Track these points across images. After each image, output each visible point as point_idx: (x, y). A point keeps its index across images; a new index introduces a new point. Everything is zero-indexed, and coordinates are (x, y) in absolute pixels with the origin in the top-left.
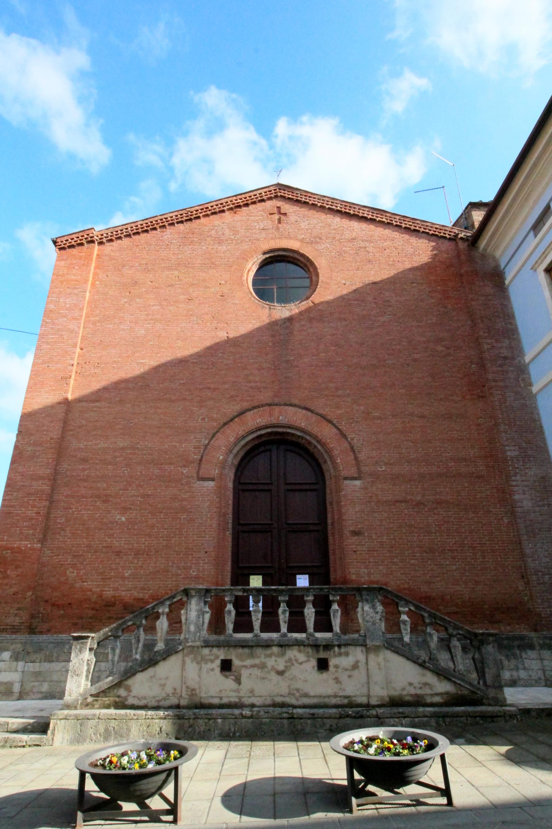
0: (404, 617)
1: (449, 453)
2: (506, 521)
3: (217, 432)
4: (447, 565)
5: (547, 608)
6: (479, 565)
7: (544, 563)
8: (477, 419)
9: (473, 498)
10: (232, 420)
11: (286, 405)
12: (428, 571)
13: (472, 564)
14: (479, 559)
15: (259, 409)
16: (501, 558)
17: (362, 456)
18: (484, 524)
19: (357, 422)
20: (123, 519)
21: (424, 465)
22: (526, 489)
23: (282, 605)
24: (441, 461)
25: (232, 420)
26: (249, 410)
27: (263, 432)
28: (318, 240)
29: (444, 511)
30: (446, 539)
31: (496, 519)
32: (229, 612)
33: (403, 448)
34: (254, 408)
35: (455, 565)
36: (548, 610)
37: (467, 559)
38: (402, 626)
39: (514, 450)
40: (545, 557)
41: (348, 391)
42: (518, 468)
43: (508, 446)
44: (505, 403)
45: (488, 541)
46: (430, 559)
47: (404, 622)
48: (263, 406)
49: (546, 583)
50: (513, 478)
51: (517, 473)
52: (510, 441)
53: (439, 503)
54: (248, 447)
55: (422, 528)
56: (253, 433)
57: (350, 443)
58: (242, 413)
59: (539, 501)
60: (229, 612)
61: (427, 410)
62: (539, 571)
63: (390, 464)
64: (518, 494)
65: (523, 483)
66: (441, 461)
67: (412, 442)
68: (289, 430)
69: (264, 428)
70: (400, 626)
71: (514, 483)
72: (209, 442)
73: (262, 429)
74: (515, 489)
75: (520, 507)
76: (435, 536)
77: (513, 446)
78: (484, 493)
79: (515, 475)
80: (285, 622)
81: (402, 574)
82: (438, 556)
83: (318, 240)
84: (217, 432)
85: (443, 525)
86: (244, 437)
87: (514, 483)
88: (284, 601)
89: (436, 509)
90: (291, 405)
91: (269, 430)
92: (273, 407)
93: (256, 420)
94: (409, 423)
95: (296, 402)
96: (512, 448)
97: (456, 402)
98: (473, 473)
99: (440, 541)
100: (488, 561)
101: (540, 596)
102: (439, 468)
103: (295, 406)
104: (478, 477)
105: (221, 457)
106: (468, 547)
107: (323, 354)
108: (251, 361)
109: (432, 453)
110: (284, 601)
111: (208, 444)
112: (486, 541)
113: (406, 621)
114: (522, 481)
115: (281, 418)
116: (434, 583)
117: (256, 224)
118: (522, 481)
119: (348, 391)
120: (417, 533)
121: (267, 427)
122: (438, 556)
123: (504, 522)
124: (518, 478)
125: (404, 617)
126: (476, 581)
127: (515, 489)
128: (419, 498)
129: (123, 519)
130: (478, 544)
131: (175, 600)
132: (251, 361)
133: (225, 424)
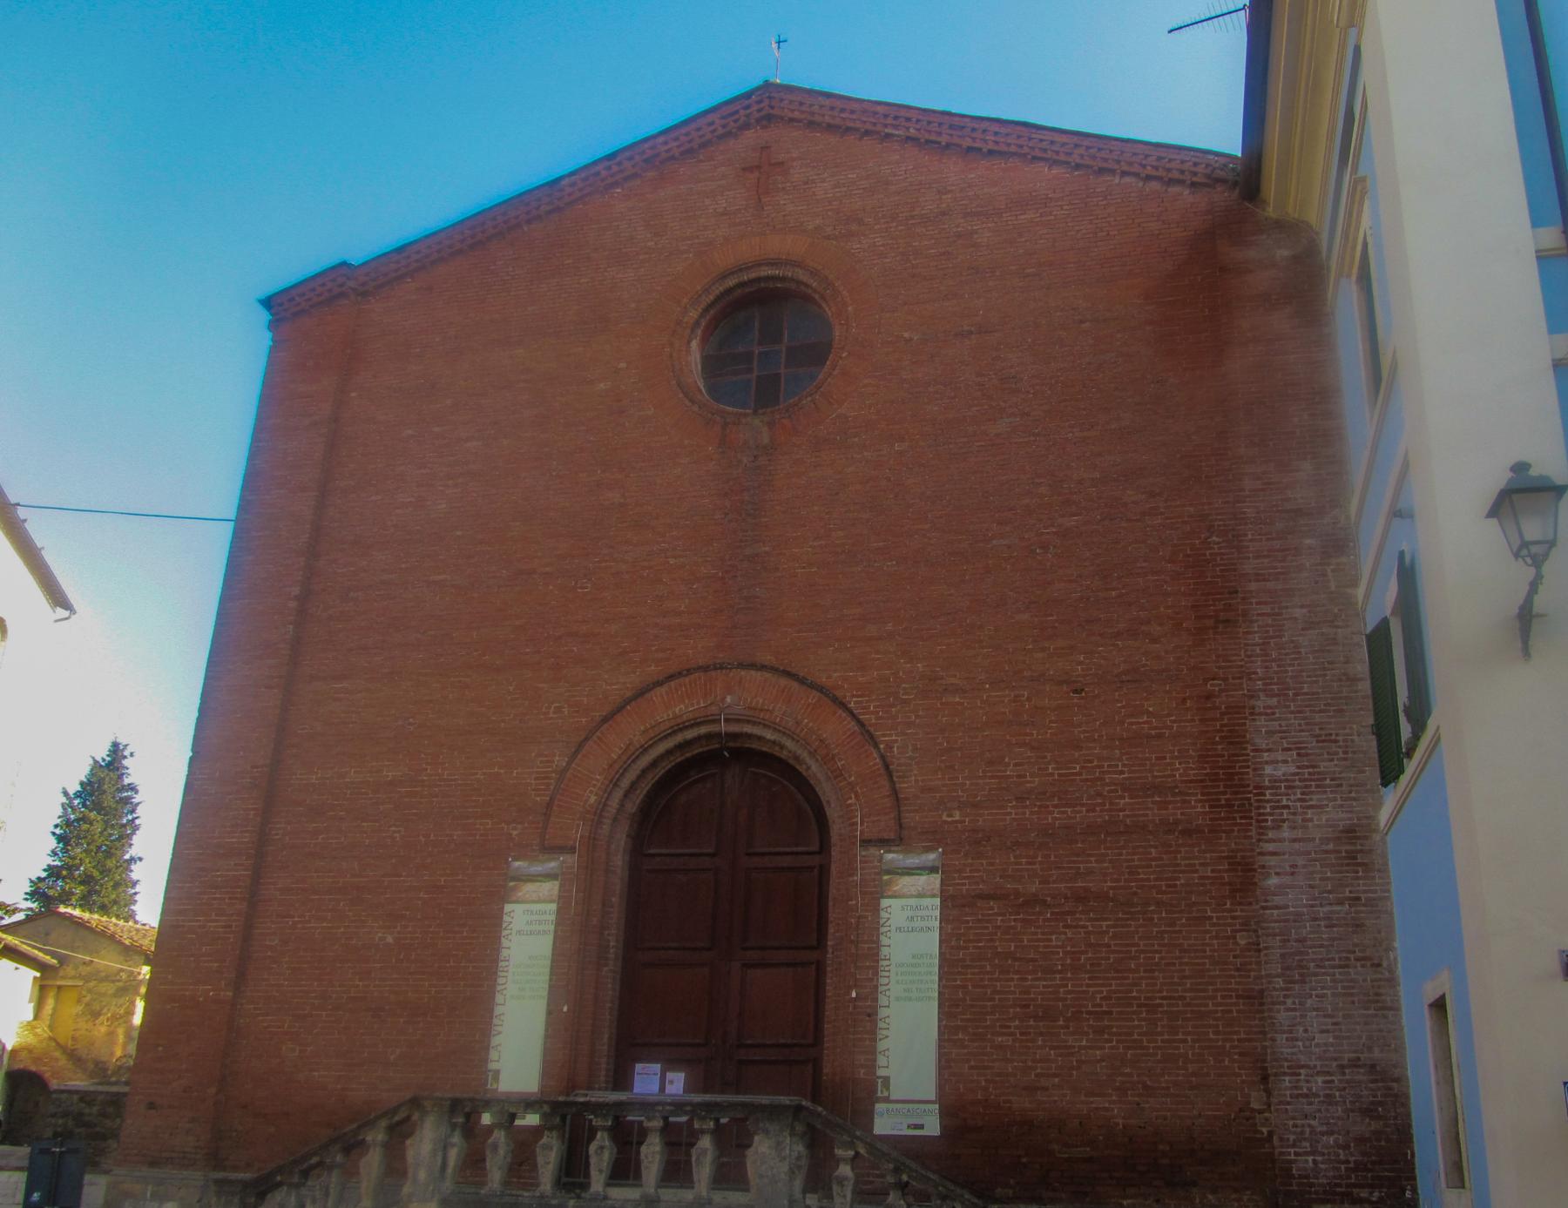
0: (845, 1170)
1: (1122, 772)
2: (1243, 942)
3: (586, 739)
4: (1080, 1047)
5: (1307, 1154)
6: (1159, 1048)
7: (1317, 1045)
8: (1206, 681)
9: (1169, 886)
10: (620, 709)
11: (741, 666)
12: (1034, 1061)
13: (1142, 1048)
14: (1161, 1034)
15: (681, 680)
16: (1217, 1033)
17: (908, 787)
18: (1185, 951)
19: (905, 702)
20: (390, 939)
21: (1056, 806)
22: (1300, 861)
23: (599, 1135)
24: (1099, 794)
25: (620, 709)
26: (659, 684)
27: (690, 734)
28: (854, 227)
29: (1090, 920)
30: (1088, 986)
31: (1217, 937)
32: (705, 1151)
33: (1008, 765)
34: (671, 677)
35: (1102, 1048)
36: (1310, 1158)
37: (1131, 1034)
38: (835, 1188)
39: (1286, 762)
40: (1322, 1032)
41: (889, 627)
42: (1288, 807)
43: (1269, 750)
44: (1280, 637)
45: (1191, 990)
46: (1041, 1034)
47: (841, 1181)
48: (689, 672)
49: (1316, 1095)
50: (1271, 835)
51: (1284, 821)
52: (1276, 737)
53: (1081, 897)
54: (660, 772)
55: (1033, 960)
56: (666, 737)
57: (883, 757)
58: (641, 693)
59: (1329, 892)
60: (495, 1147)
61: (1081, 663)
62: (1303, 1067)
63: (975, 806)
64: (1277, 874)
65: (1296, 845)
66: (1099, 794)
67: (1033, 748)
68: (748, 729)
69: (692, 726)
70: (830, 1189)
71: (1270, 847)
72: (569, 764)
73: (686, 728)
74: (1272, 861)
75: (1277, 908)
76: (1062, 979)
77: (1285, 750)
78: (1196, 871)
79: (1277, 826)
80: (601, 1171)
81: (971, 1068)
82: (1062, 1027)
83: (854, 227)
84: (586, 739)
85: (1086, 952)
86: (645, 750)
87: (1270, 847)
88: (604, 1128)
89: (1071, 913)
90: (753, 666)
91: (703, 730)
92: (713, 673)
93: (675, 707)
94: (1029, 699)
95: (768, 658)
96: (1280, 756)
97: (1154, 640)
98: (1177, 822)
99: (1069, 992)
100: (1185, 1041)
101: (1295, 1126)
102: (1094, 811)
103: (763, 667)
104: (1187, 833)
105: (593, 799)
106: (1139, 1006)
107: (840, 533)
108: (672, 561)
109: (1080, 774)
110: (604, 1128)
111: (565, 770)
112: (1185, 991)
113: (846, 1178)
114: (1294, 840)
115: (729, 699)
116: (1047, 1089)
117: (707, 202)
118: (1294, 840)
119: (889, 627)
120: (1018, 972)
121: (696, 724)
122: (1062, 1027)
123: (1236, 943)
124: (1286, 833)
125: (845, 1170)
126: (1145, 1087)
127: (1272, 861)
128: (1034, 887)
129: (390, 939)
130: (1163, 998)
131: (397, 1118)
132: (672, 561)
133: (605, 720)
